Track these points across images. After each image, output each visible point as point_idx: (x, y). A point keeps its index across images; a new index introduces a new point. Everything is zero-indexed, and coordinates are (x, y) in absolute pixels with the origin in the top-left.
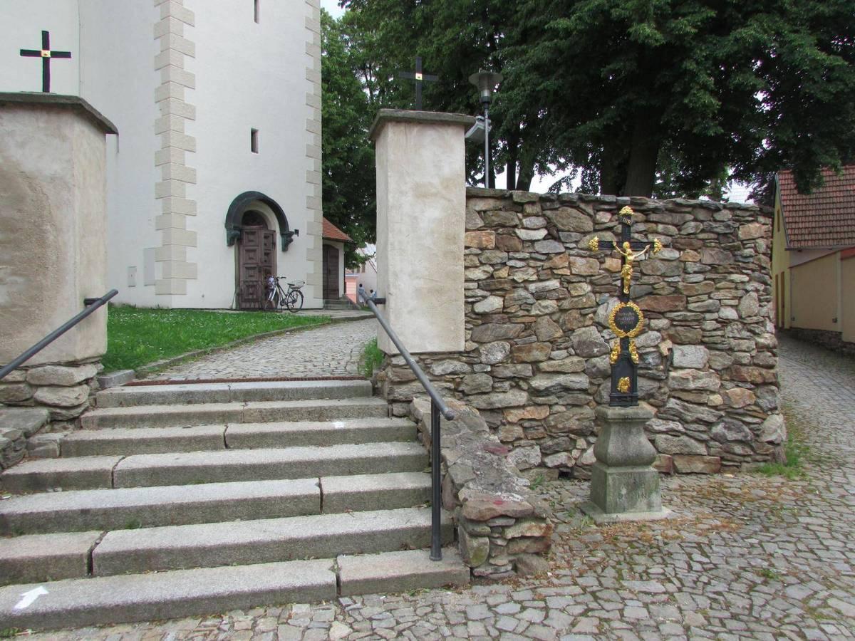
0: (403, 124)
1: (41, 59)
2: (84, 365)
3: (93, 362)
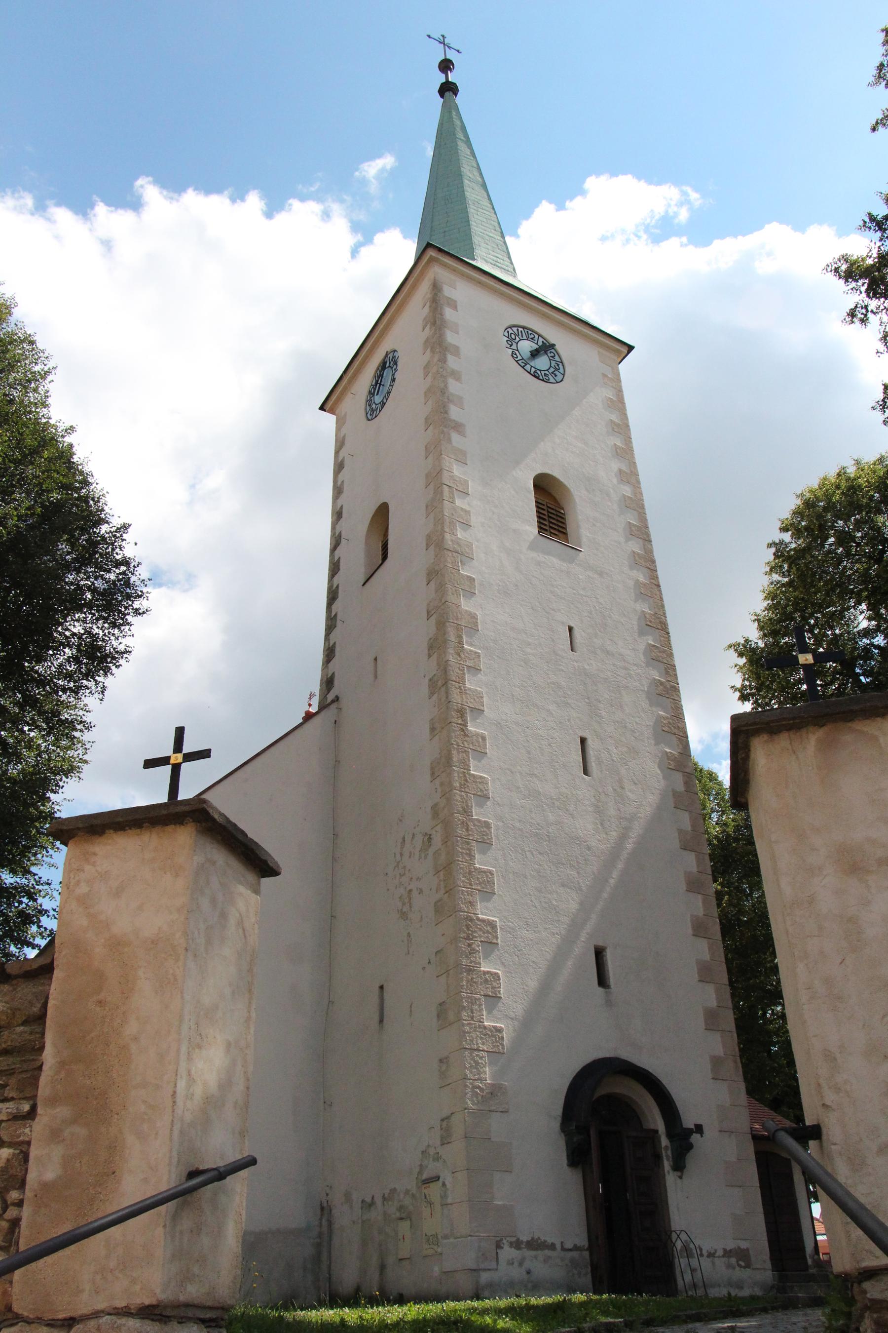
0: (784, 735)
1: (170, 767)
2: (182, 1320)
3: (203, 1321)
